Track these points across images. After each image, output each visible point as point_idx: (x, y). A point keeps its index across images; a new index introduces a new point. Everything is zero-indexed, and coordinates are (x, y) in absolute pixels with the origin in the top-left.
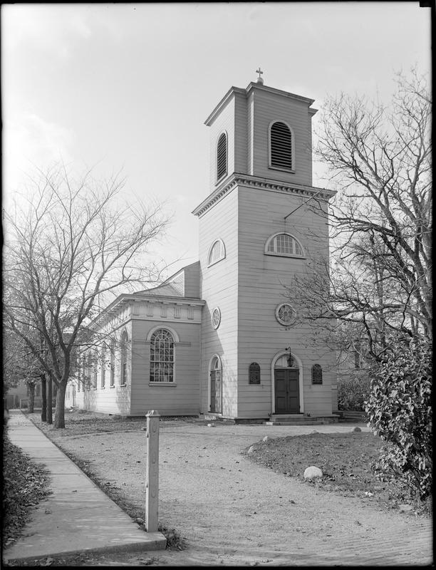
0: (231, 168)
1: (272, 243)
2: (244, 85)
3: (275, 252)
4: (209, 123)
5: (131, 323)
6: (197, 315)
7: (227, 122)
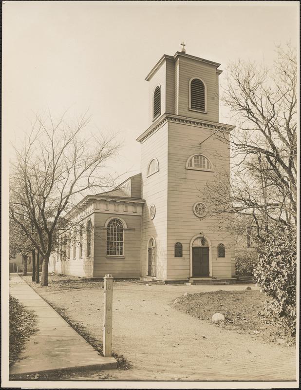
0: (163, 110)
1: (191, 161)
2: (172, 54)
3: (193, 167)
4: (148, 79)
5: (94, 215)
6: (139, 210)
7: (160, 78)
